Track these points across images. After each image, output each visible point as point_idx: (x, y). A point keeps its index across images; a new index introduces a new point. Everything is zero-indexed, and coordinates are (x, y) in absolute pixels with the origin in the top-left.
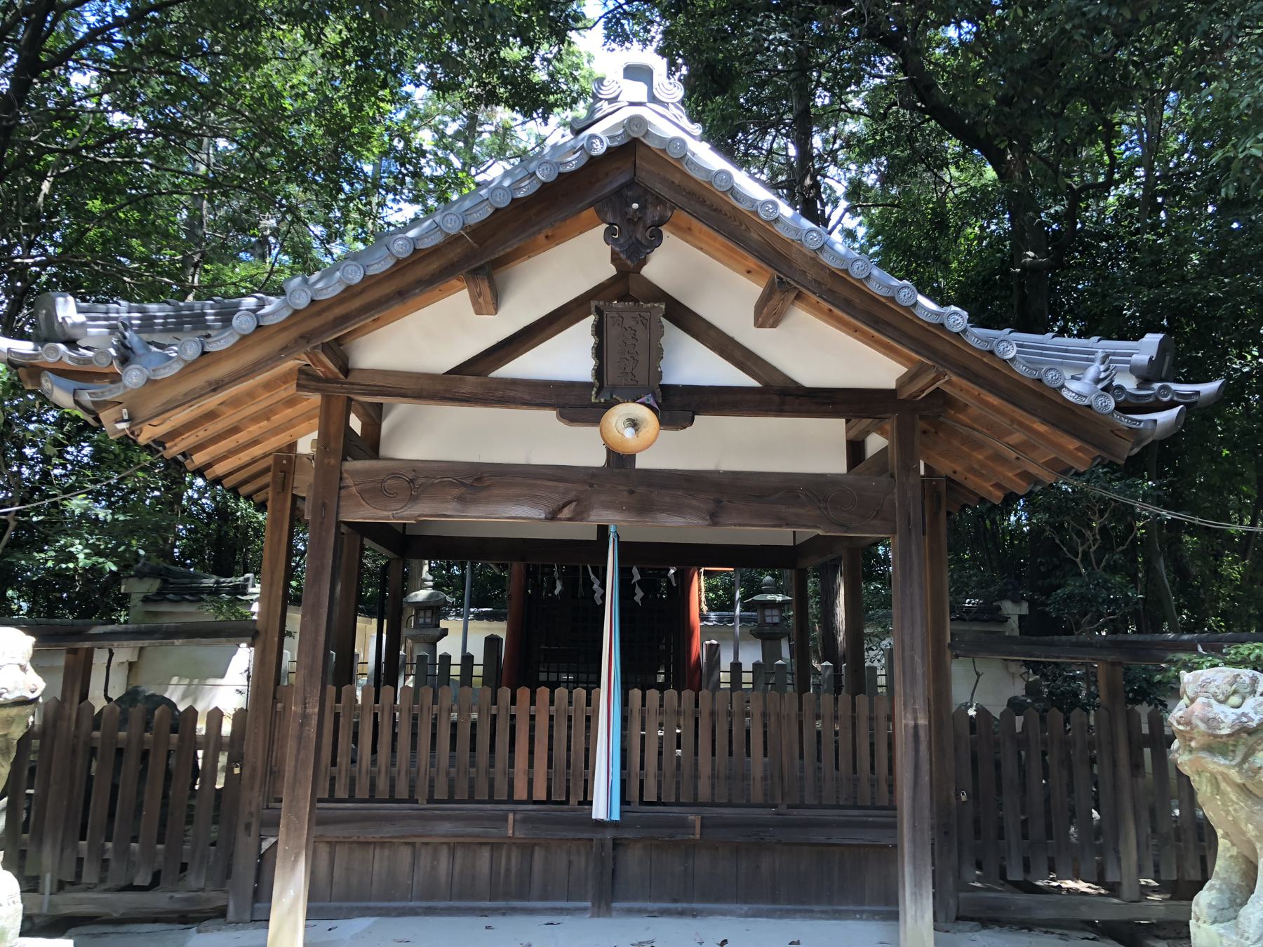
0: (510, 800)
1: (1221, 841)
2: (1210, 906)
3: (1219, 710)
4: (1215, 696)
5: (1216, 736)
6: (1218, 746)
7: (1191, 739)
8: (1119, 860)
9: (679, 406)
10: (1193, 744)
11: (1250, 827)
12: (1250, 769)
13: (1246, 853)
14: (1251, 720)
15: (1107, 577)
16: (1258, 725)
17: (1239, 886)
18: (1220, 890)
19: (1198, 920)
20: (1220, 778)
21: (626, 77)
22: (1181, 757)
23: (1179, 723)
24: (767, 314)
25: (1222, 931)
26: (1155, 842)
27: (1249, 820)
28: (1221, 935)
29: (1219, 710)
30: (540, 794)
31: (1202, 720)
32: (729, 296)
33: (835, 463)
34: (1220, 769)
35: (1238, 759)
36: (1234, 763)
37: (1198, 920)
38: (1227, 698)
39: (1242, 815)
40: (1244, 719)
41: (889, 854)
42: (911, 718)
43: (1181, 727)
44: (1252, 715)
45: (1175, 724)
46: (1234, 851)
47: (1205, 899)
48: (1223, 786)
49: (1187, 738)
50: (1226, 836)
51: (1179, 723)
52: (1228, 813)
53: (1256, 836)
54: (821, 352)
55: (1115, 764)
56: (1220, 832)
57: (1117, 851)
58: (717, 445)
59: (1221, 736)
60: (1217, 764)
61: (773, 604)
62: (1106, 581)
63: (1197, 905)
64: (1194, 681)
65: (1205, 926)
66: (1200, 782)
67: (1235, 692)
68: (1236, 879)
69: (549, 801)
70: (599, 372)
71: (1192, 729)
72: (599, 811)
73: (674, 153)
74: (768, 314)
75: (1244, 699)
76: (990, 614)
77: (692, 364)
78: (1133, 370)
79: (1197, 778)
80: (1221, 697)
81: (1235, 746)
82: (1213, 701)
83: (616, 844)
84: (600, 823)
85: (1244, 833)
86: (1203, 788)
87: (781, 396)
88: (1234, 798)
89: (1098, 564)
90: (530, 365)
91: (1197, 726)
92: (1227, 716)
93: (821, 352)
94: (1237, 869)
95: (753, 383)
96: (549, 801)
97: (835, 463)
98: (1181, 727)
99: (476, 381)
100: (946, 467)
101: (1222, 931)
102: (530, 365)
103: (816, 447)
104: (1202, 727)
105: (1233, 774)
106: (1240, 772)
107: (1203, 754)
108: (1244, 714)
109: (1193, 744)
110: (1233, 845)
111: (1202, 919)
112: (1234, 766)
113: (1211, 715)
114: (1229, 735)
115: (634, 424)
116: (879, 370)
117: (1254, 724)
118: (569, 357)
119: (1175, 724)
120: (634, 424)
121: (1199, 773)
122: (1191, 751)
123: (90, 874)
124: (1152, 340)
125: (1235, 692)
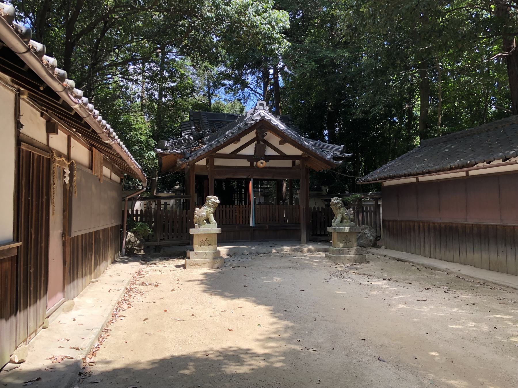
0: (236, 224)
6: (334, 205)
9: (268, 158)
21: (280, 144)
24: (281, 143)
30: (241, 223)
32: (275, 140)
33: (291, 165)
41: (299, 231)
42: (303, 207)
54: (289, 150)
58: (273, 163)
61: (267, 188)
69: (243, 224)
70: (255, 154)
72: (251, 225)
73: (269, 122)
74: (281, 143)
76: (319, 189)
77: (270, 152)
78: (339, 151)
83: (254, 230)
84: (251, 227)
87: (283, 156)
90: (243, 152)
93: (289, 150)
95: (278, 154)
96: (243, 224)
97: (291, 165)
99: (234, 155)
100: (309, 165)
102: (243, 152)
103: (288, 163)
115: (262, 163)
116: (299, 153)
118: (250, 151)
120: (262, 163)
123: (166, 238)
124: (342, 146)
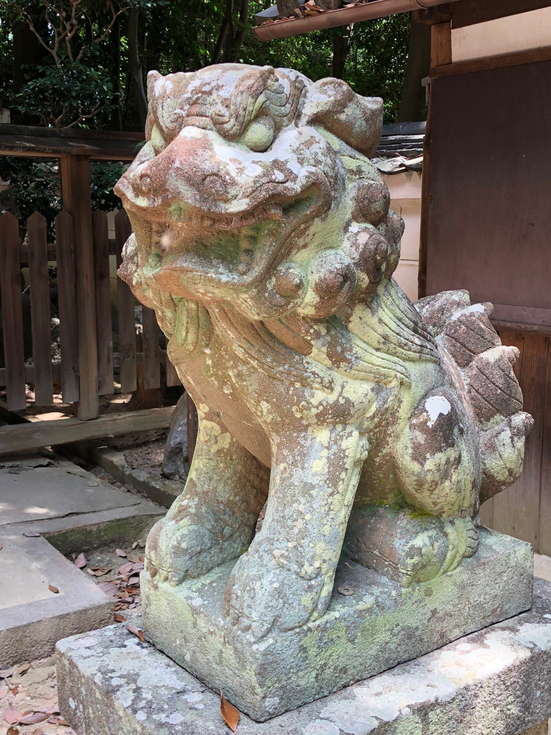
1: (203, 424)
2: (177, 551)
3: (225, 156)
4: (217, 124)
5: (216, 218)
6: (220, 238)
7: (163, 228)
8: (78, 378)
10: (166, 241)
11: (265, 406)
12: (278, 290)
13: (248, 446)
14: (291, 176)
15: (81, 67)
16: (306, 189)
17: (229, 504)
18: (197, 518)
19: (154, 574)
20: (215, 311)
22: (141, 272)
23: (138, 191)
25: (197, 602)
26: (116, 355)
27: (263, 393)
28: (195, 611)
29: (225, 156)
31: (189, 180)
34: (219, 293)
35: (257, 270)
36: (248, 279)
37: (154, 574)
38: (245, 127)
39: (252, 385)
40: (279, 176)
43: (142, 202)
44: (293, 166)
45: (130, 194)
46: (225, 442)
47: (171, 533)
48: (221, 328)
49: (155, 225)
50: (211, 416)
51: (138, 191)
52: (224, 380)
53: (274, 423)
55: (77, 273)
56: (202, 410)
57: (76, 370)
59: (228, 218)
60: (216, 282)
62: (80, 72)
63: (155, 547)
64: (177, 93)
65: (164, 586)
66: (175, 322)
67: (261, 113)
68: (224, 493)
71: (166, 203)
75: (277, 129)
79: (169, 314)
80: (231, 125)
81: (253, 239)
82: (213, 136)
85: (248, 416)
86: (181, 339)
88: (240, 352)
89: (75, 56)
91: (177, 195)
92: (241, 168)
94: (228, 473)
98: (142, 202)
101: (197, 602)
104: (189, 196)
105: (248, 307)
106: (257, 299)
107: (186, 263)
108: (277, 164)
109: (166, 241)
110: (224, 429)
111: (163, 573)
112: (248, 287)
113: (208, 167)
114: (244, 215)
117: (296, 187)
119: (130, 194)
121: (173, 304)
122: (161, 255)
125: (261, 113)
